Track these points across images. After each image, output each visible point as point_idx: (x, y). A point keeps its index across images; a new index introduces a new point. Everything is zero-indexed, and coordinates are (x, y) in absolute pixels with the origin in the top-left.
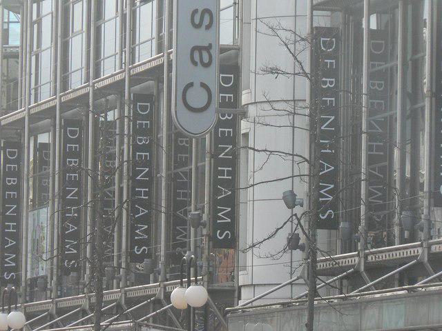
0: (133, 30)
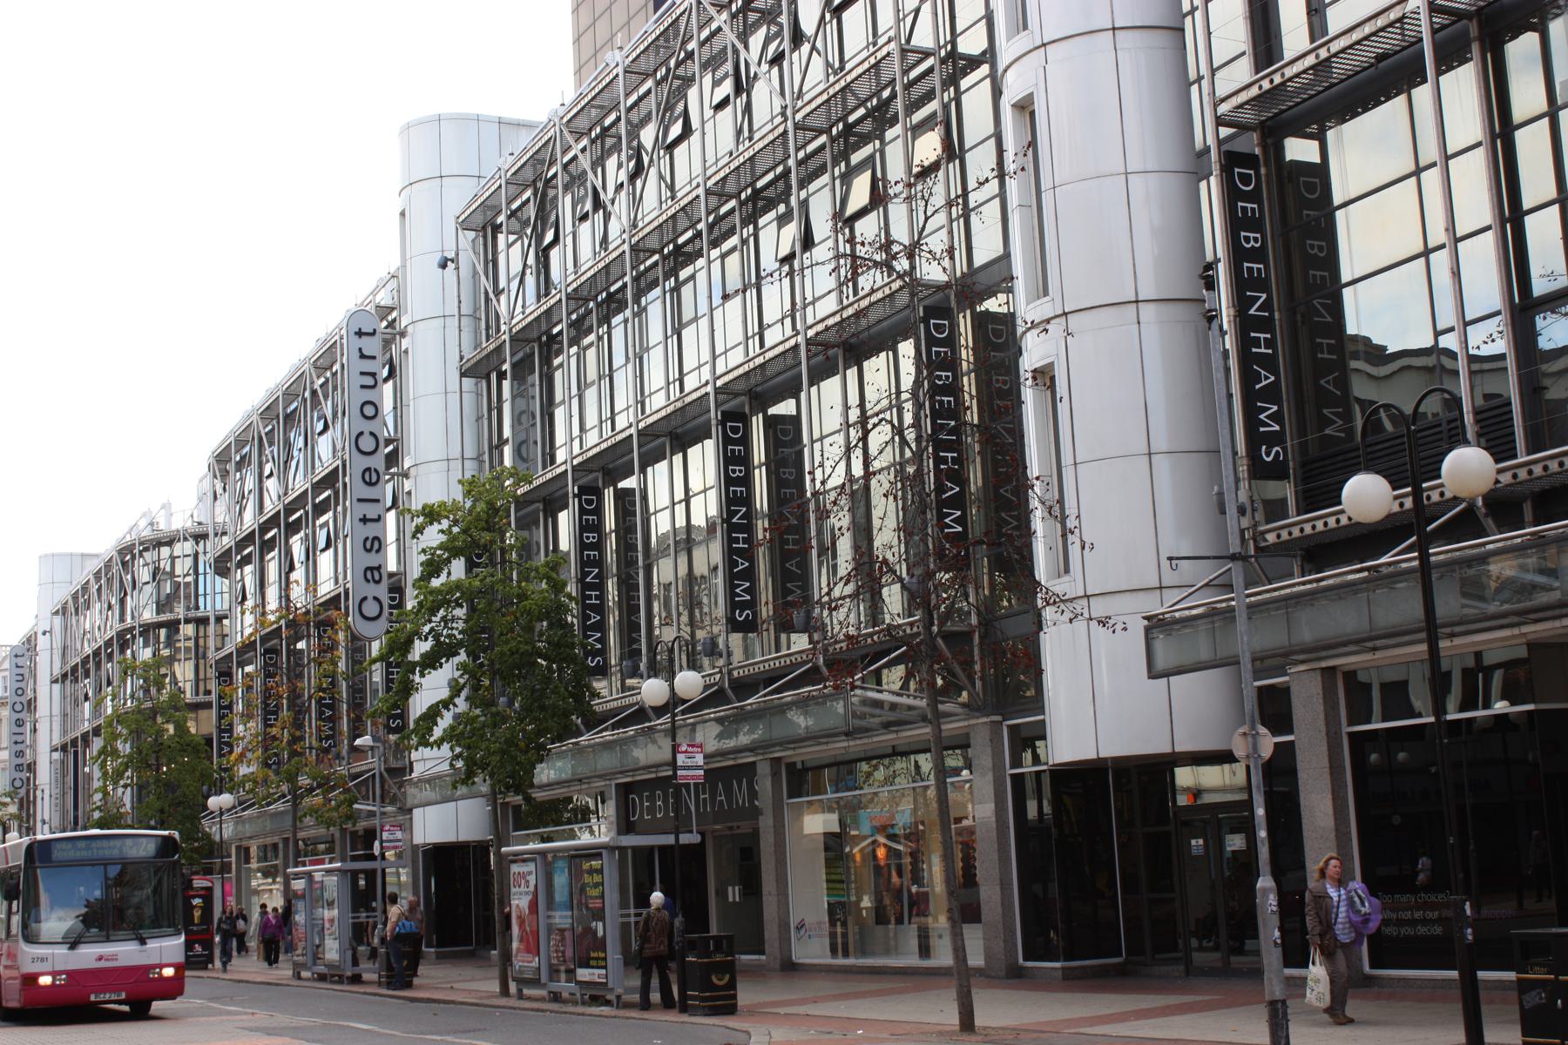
0: (315, 571)
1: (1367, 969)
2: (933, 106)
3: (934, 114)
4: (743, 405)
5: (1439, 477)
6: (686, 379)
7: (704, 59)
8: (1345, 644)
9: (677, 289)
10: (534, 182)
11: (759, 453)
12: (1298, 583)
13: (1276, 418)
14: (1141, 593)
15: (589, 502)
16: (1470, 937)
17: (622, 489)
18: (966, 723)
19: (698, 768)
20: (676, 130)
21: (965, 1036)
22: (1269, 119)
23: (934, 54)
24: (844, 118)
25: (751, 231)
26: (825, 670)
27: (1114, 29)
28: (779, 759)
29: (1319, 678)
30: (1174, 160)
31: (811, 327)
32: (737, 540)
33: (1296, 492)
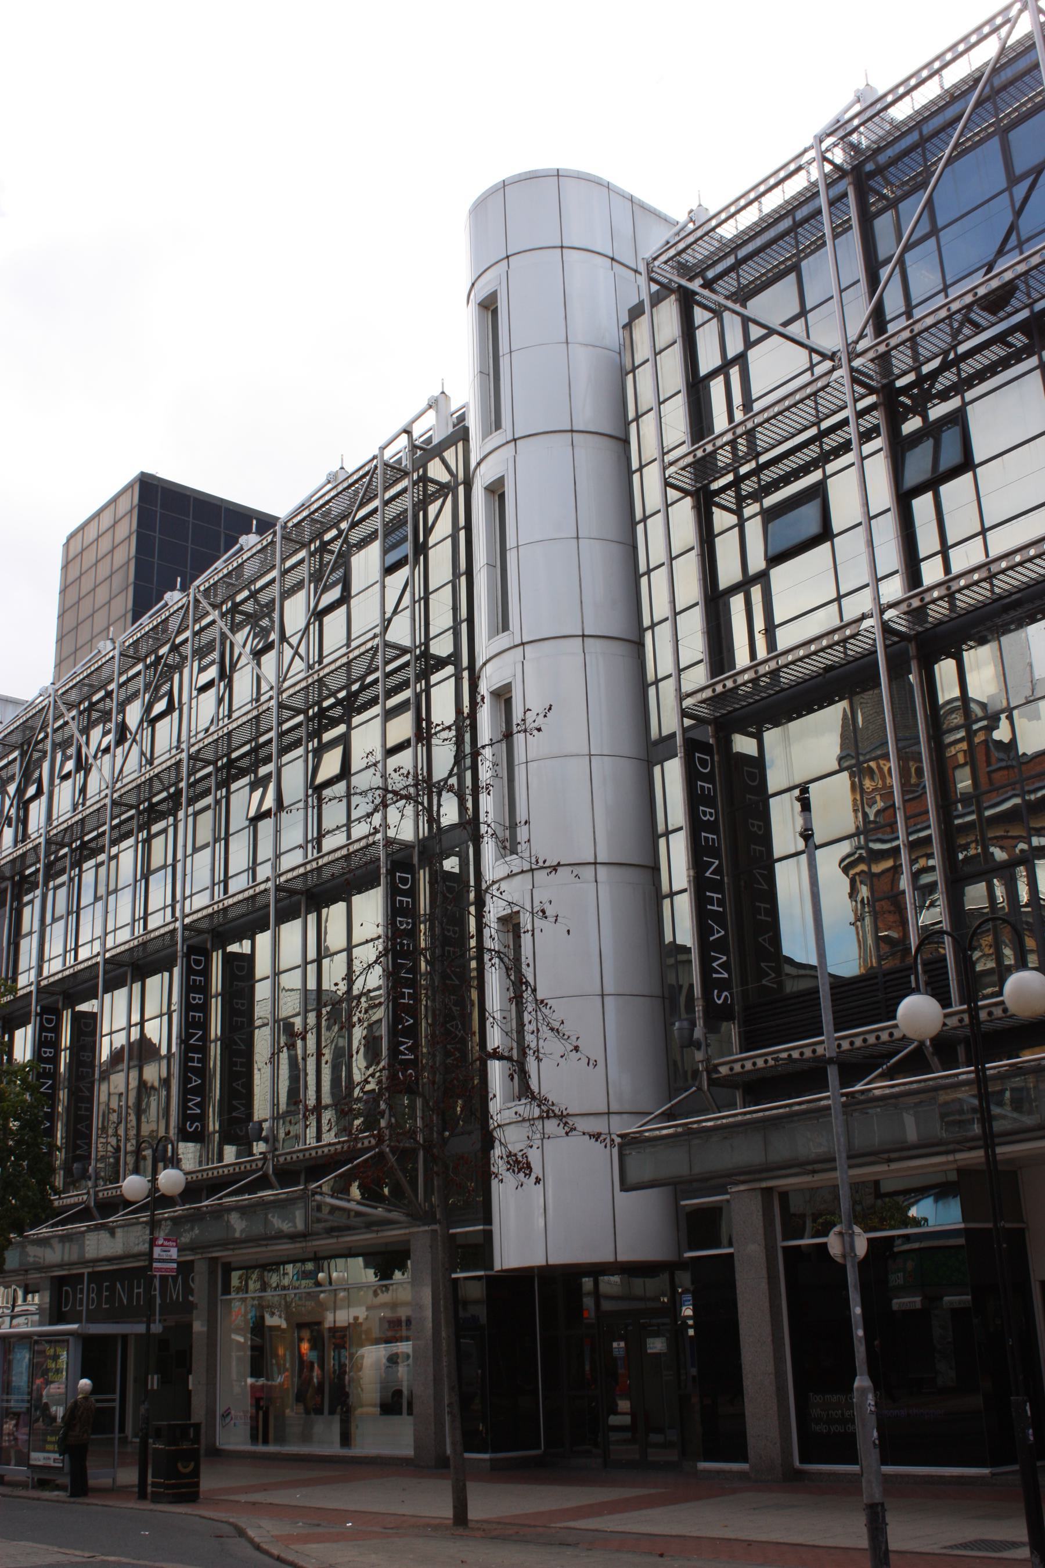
1: (797, 1464)
2: (406, 694)
3: (409, 700)
4: (206, 942)
5: (894, 1018)
6: (80, 950)
7: (121, 699)
8: (214, 1246)
9: (148, 841)
10: (22, 745)
11: (66, 1039)
12: (740, 1113)
13: (725, 966)
14: (591, 1118)
15: (49, 1021)
16: (1031, 1438)
17: (80, 1012)
18: (407, 1231)
19: (172, 1261)
20: (160, 706)
21: (460, 1531)
22: (723, 715)
23: (410, 652)
24: (228, 755)
25: (224, 794)
26: (273, 1179)
27: (583, 636)
28: (217, 1258)
29: (760, 1197)
30: (627, 745)
31: (188, 916)
32: (192, 1060)
33: (739, 1032)
